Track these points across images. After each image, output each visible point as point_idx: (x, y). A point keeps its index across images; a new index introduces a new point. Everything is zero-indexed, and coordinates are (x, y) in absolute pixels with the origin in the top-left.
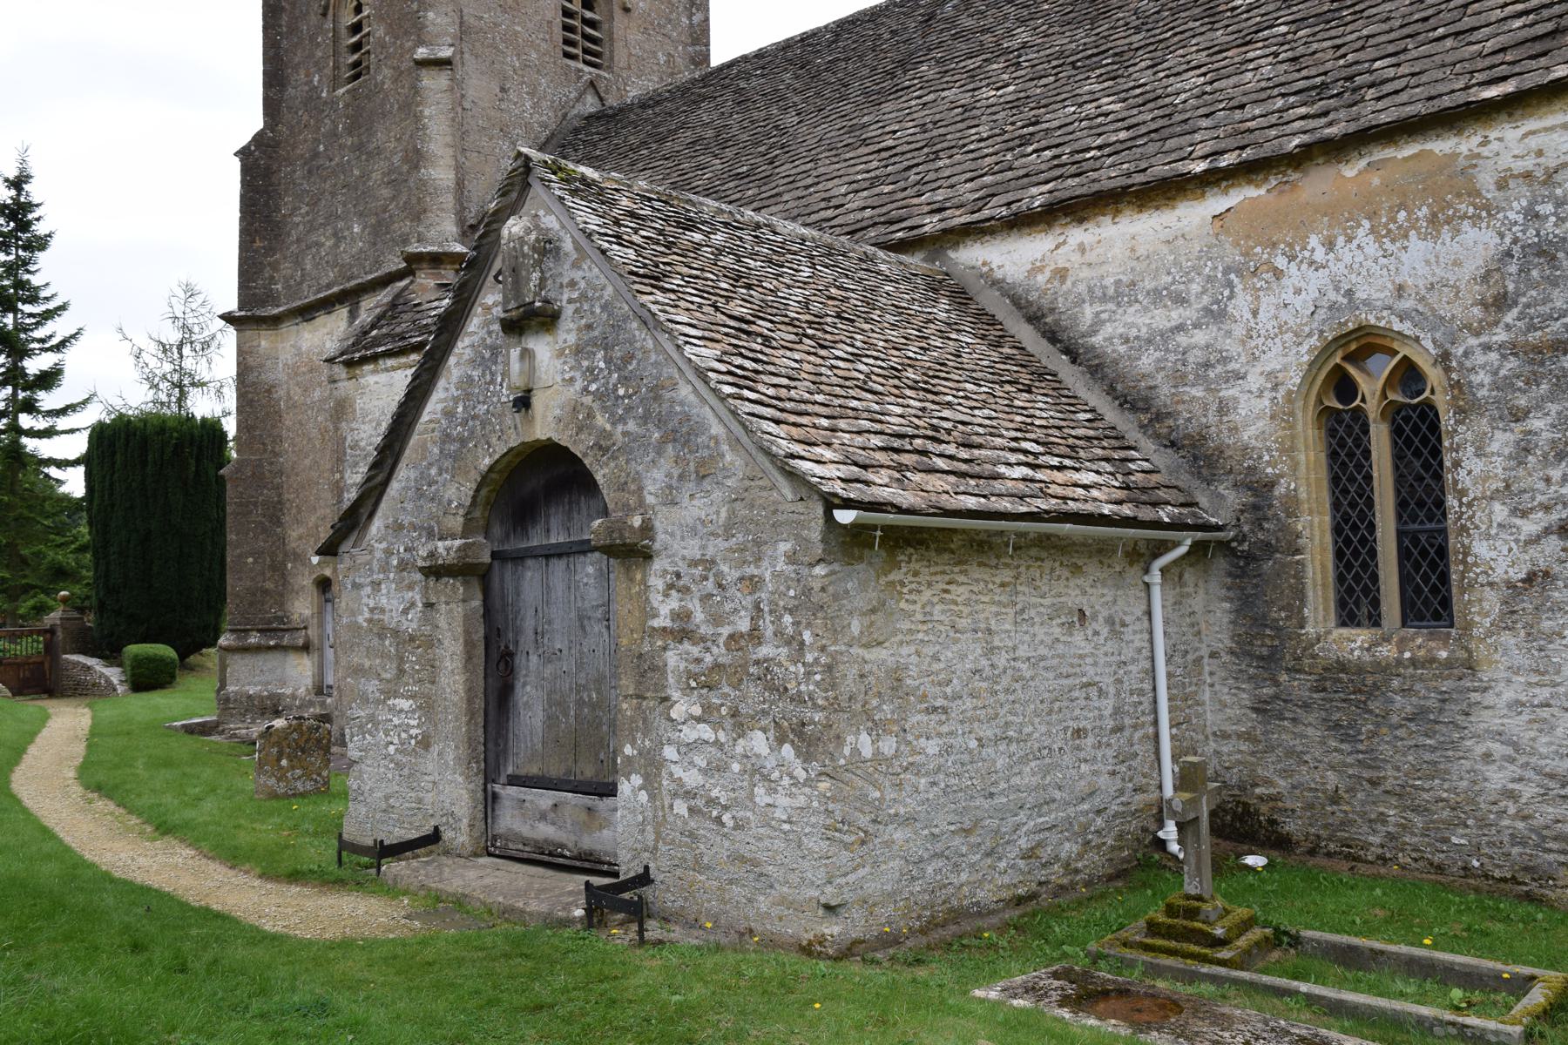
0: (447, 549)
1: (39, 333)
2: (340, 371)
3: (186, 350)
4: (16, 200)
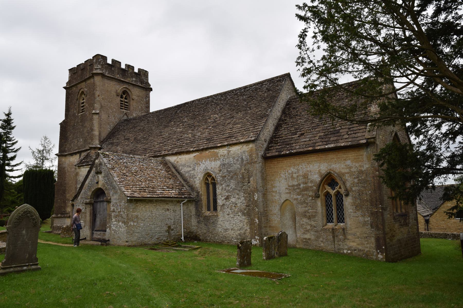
0: (88, 201)
1: (10, 148)
2: (77, 167)
3: (44, 152)
4: (7, 119)
